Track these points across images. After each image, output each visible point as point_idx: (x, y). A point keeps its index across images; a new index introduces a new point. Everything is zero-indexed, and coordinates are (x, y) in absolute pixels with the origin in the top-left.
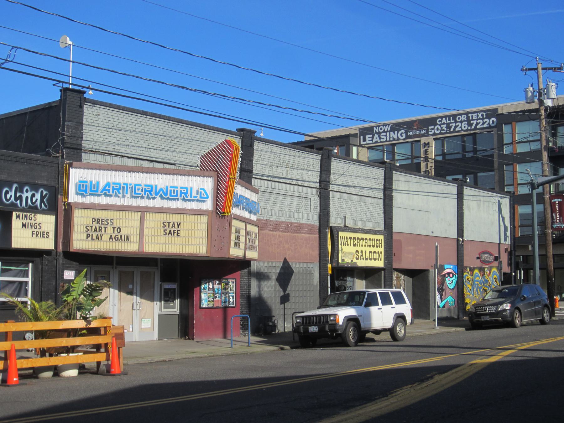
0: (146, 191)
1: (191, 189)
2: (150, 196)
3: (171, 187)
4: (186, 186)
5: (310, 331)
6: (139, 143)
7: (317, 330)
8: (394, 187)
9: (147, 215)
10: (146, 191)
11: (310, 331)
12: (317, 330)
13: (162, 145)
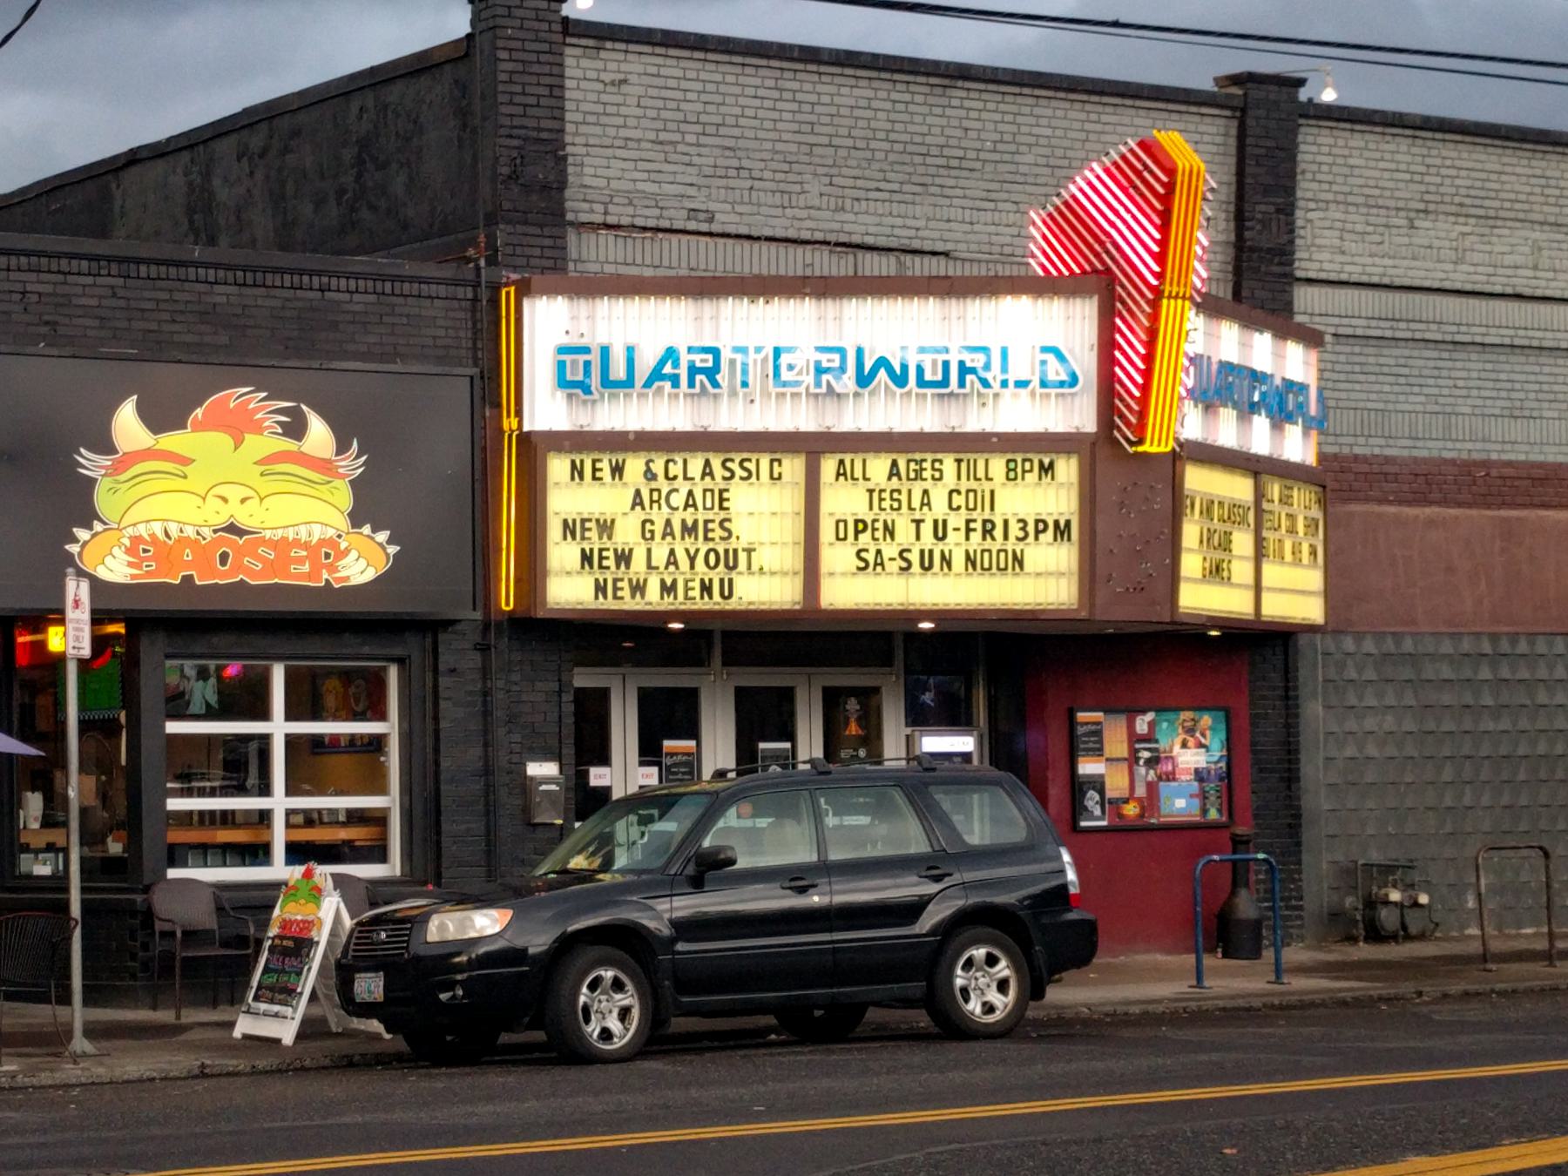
0: (820, 370)
6: (791, 177)
13: (890, 176)
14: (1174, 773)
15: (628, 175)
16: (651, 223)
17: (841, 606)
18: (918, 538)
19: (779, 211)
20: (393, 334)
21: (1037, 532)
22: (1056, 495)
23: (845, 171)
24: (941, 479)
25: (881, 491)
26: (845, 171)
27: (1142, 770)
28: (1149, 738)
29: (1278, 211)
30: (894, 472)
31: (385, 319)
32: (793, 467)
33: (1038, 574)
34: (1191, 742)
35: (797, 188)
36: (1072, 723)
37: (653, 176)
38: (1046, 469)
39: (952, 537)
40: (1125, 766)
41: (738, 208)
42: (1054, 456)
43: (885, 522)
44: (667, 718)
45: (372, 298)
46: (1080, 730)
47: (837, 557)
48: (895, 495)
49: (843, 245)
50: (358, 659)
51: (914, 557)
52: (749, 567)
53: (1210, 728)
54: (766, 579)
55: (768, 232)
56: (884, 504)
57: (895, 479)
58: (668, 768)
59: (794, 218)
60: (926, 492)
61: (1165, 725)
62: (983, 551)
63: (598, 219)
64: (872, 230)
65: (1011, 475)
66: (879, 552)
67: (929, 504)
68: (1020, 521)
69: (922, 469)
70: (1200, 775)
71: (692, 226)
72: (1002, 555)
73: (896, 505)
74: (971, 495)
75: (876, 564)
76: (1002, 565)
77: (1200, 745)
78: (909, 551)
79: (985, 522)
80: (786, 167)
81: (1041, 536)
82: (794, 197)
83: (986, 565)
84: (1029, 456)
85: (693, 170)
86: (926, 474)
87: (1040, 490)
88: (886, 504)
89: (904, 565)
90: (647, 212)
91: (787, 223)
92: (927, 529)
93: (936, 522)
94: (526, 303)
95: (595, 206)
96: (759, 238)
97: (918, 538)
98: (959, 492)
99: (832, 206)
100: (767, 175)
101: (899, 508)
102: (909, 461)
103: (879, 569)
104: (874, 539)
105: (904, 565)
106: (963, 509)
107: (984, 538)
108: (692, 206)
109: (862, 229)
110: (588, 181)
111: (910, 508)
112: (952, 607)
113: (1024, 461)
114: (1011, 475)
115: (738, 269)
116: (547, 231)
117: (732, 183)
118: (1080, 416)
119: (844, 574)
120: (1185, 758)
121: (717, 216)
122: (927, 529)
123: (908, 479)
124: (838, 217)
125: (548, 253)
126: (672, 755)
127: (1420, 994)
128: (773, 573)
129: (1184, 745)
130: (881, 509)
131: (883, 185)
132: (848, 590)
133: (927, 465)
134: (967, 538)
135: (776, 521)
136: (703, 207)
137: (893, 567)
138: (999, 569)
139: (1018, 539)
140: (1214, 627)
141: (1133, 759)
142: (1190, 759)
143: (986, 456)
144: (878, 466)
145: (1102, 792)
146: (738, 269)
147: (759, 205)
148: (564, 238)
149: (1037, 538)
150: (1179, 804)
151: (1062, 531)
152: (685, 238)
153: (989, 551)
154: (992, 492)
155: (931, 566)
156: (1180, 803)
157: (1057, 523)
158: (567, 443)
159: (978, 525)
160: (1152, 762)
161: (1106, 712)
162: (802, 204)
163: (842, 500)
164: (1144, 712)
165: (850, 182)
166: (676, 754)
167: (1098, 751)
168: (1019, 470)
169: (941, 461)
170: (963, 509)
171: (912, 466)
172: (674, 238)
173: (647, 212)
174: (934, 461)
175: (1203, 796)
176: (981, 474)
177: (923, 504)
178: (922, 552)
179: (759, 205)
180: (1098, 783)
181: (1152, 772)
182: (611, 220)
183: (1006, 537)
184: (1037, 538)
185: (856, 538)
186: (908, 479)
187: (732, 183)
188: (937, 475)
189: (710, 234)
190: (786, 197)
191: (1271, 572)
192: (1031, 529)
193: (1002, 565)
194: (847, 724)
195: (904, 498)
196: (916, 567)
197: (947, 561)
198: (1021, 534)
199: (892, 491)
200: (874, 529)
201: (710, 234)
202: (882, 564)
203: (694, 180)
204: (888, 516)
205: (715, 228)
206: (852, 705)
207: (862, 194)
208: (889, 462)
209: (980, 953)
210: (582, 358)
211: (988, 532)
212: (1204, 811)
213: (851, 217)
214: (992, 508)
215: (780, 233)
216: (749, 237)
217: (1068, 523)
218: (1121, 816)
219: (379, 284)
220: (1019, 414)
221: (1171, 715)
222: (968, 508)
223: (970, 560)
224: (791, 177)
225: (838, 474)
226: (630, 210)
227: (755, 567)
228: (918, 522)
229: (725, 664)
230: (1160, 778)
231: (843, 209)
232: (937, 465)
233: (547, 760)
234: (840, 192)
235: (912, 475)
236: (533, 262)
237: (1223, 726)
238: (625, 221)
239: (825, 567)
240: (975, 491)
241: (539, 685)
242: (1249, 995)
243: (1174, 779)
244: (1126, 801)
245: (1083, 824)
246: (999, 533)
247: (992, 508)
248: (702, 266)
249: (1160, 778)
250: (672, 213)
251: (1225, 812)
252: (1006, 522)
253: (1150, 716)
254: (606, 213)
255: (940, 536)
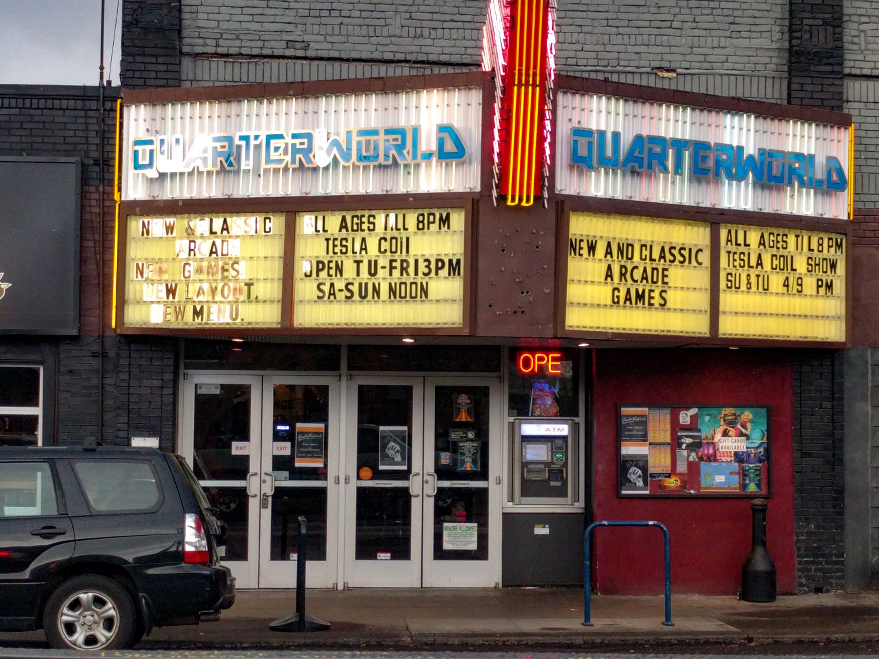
0: (295, 151)
1: (416, 130)
2: (306, 165)
3: (362, 133)
4: (403, 123)
5: (536, 533)
6: (375, 15)
7: (235, 444)
8: (853, 62)
9: (307, 222)
10: (295, 151)
11: (536, 533)
12: (235, 444)
13: (463, 10)
14: (715, 455)
15: (234, 18)
16: (255, 52)
17: (307, 326)
18: (358, 274)
19: (366, 40)
20: (31, 135)
21: (437, 269)
22: (448, 242)
23: (422, 8)
24: (374, 230)
25: (335, 239)
26: (422, 8)
27: (685, 453)
28: (693, 426)
29: (826, 23)
30: (343, 226)
31: (24, 126)
32: (276, 223)
33: (438, 301)
34: (732, 432)
35: (382, 22)
36: (618, 417)
37: (256, 18)
38: (445, 221)
39: (381, 273)
40: (668, 449)
41: (329, 39)
42: (450, 210)
43: (337, 262)
44: (302, 408)
45: (17, 111)
46: (624, 421)
47: (305, 289)
48: (344, 243)
49: (423, 62)
50: (20, 363)
51: (355, 288)
52: (249, 297)
53: (751, 421)
54: (260, 306)
55: (355, 55)
56: (736, 264)
57: (344, 230)
58: (300, 443)
59: (378, 44)
60: (364, 240)
61: (707, 418)
62: (401, 283)
63: (211, 50)
64: (446, 50)
65: (421, 226)
66: (332, 285)
67: (365, 249)
68: (426, 260)
69: (362, 223)
70: (739, 457)
71: (290, 52)
72: (414, 286)
73: (344, 250)
74: (394, 241)
75: (330, 294)
76: (413, 295)
77: (741, 434)
78: (352, 284)
79: (402, 261)
80: (372, 7)
81: (440, 272)
82: (378, 29)
83: (403, 295)
84: (432, 211)
85: (293, 13)
86: (364, 226)
87: (440, 237)
88: (337, 250)
89: (349, 294)
90: (250, 44)
91: (373, 48)
92: (364, 267)
93: (370, 262)
94: (125, 110)
95: (208, 41)
96: (348, 60)
97: (358, 274)
98: (385, 240)
99: (412, 34)
100: (356, 14)
101: (346, 253)
102: (353, 217)
103: (332, 297)
104: (329, 275)
105: (349, 294)
106: (388, 253)
107: (402, 274)
108: (291, 38)
109: (439, 50)
110: (202, 23)
111: (354, 252)
112: (358, 326)
113: (429, 215)
114: (421, 226)
115: (244, 79)
116: (160, 60)
117: (324, 21)
118: (464, 179)
119: (309, 301)
120: (731, 445)
121: (311, 44)
122: (364, 267)
123: (353, 230)
124: (416, 42)
125: (162, 75)
126: (303, 433)
127: (750, 640)
128: (264, 301)
129: (725, 434)
130: (335, 253)
131: (456, 18)
132: (315, 314)
133: (365, 219)
134: (391, 274)
135: (269, 263)
136: (300, 39)
137: (341, 296)
138: (411, 297)
139: (424, 274)
140: (585, 341)
141: (675, 444)
142: (730, 445)
143: (404, 211)
144: (333, 221)
145: (644, 469)
146: (244, 79)
147: (348, 36)
148: (180, 64)
149: (437, 274)
150: (719, 479)
151: (454, 267)
152: (283, 62)
153: (405, 283)
154: (408, 239)
155: (366, 296)
156: (720, 479)
157: (450, 261)
158: (138, 209)
159: (397, 264)
160: (696, 446)
161: (650, 406)
162: (385, 34)
163: (311, 249)
164: (688, 408)
165: (429, 16)
166: (308, 433)
167: (643, 438)
168: (426, 222)
169: (374, 217)
170: (388, 253)
171: (355, 220)
172: (275, 63)
173: (250, 44)
174: (369, 216)
175: (744, 474)
176: (741, 240)
177: (361, 249)
178: (360, 284)
179: (348, 36)
180: (641, 463)
181: (693, 454)
182: (220, 50)
183: (416, 273)
184: (437, 274)
185: (318, 275)
186: (353, 230)
187: (324, 21)
188: (371, 227)
189: (305, 58)
190: (371, 29)
191: (728, 300)
192: (433, 266)
193: (413, 295)
194: (459, 410)
195: (349, 244)
196: (356, 297)
197: (376, 291)
198: (426, 271)
199: (342, 240)
200: (330, 268)
201: (305, 58)
202: (334, 294)
203: (291, 19)
204: (338, 258)
205: (310, 53)
206: (463, 400)
207: (438, 24)
208: (340, 218)
209: (86, 596)
210: (148, 148)
211: (404, 270)
212: (744, 486)
213: (430, 42)
214: (407, 252)
215: (365, 55)
216: (341, 60)
217: (458, 261)
218: (661, 486)
219: (20, 101)
220: (433, 180)
221: (714, 411)
222: (391, 252)
223: (392, 290)
224: (375, 15)
225: (760, 244)
226: (238, 43)
227: (253, 297)
228: (358, 262)
229: (350, 368)
230: (701, 459)
231: (422, 36)
232: (372, 219)
233: (149, 436)
234: (419, 24)
235: (355, 227)
236: (149, 82)
237: (764, 421)
238: (232, 51)
239: (298, 296)
240: (396, 238)
241: (145, 382)
242: (571, 634)
243: (715, 460)
244: (669, 476)
245: (624, 492)
246: (411, 270)
247: (407, 252)
248: (221, 78)
249: (701, 459)
250: (273, 44)
251: (764, 487)
252: (416, 261)
253: (694, 411)
254: (217, 46)
255: (373, 273)
